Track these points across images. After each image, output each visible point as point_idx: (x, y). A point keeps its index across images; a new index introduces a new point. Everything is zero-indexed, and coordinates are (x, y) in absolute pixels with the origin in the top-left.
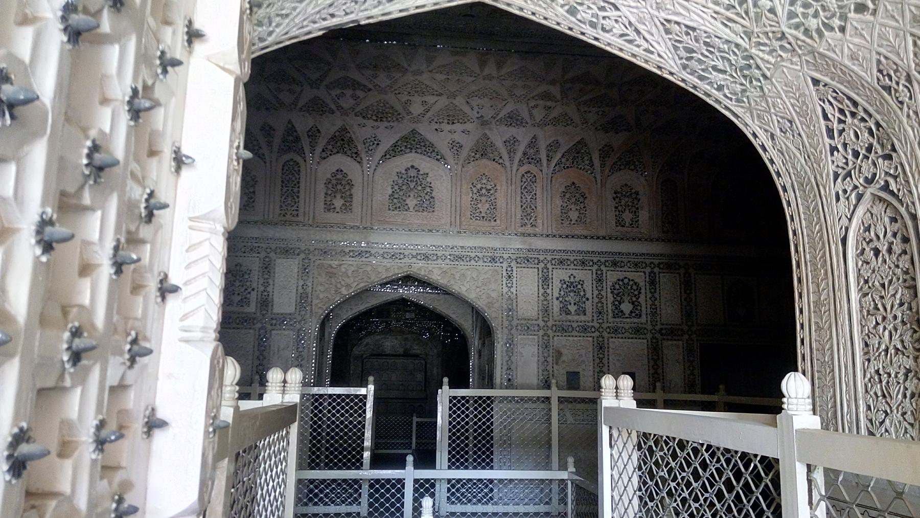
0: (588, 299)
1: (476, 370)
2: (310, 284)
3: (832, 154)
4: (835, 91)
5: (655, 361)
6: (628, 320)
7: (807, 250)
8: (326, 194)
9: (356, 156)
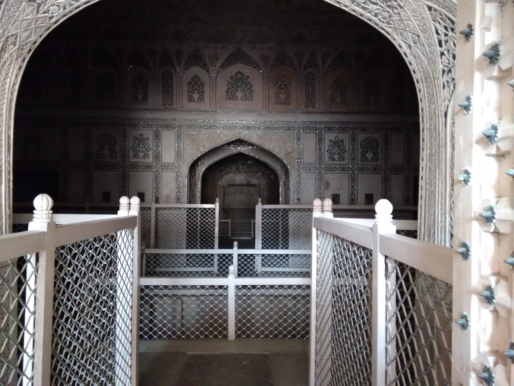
0: (150, 149)
1: (283, 194)
2: (182, 146)
3: (441, 58)
4: (441, 14)
5: (386, 187)
6: (370, 163)
7: (428, 121)
8: (189, 91)
9: (205, 67)
